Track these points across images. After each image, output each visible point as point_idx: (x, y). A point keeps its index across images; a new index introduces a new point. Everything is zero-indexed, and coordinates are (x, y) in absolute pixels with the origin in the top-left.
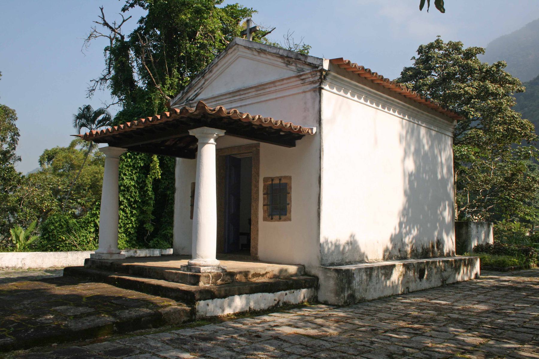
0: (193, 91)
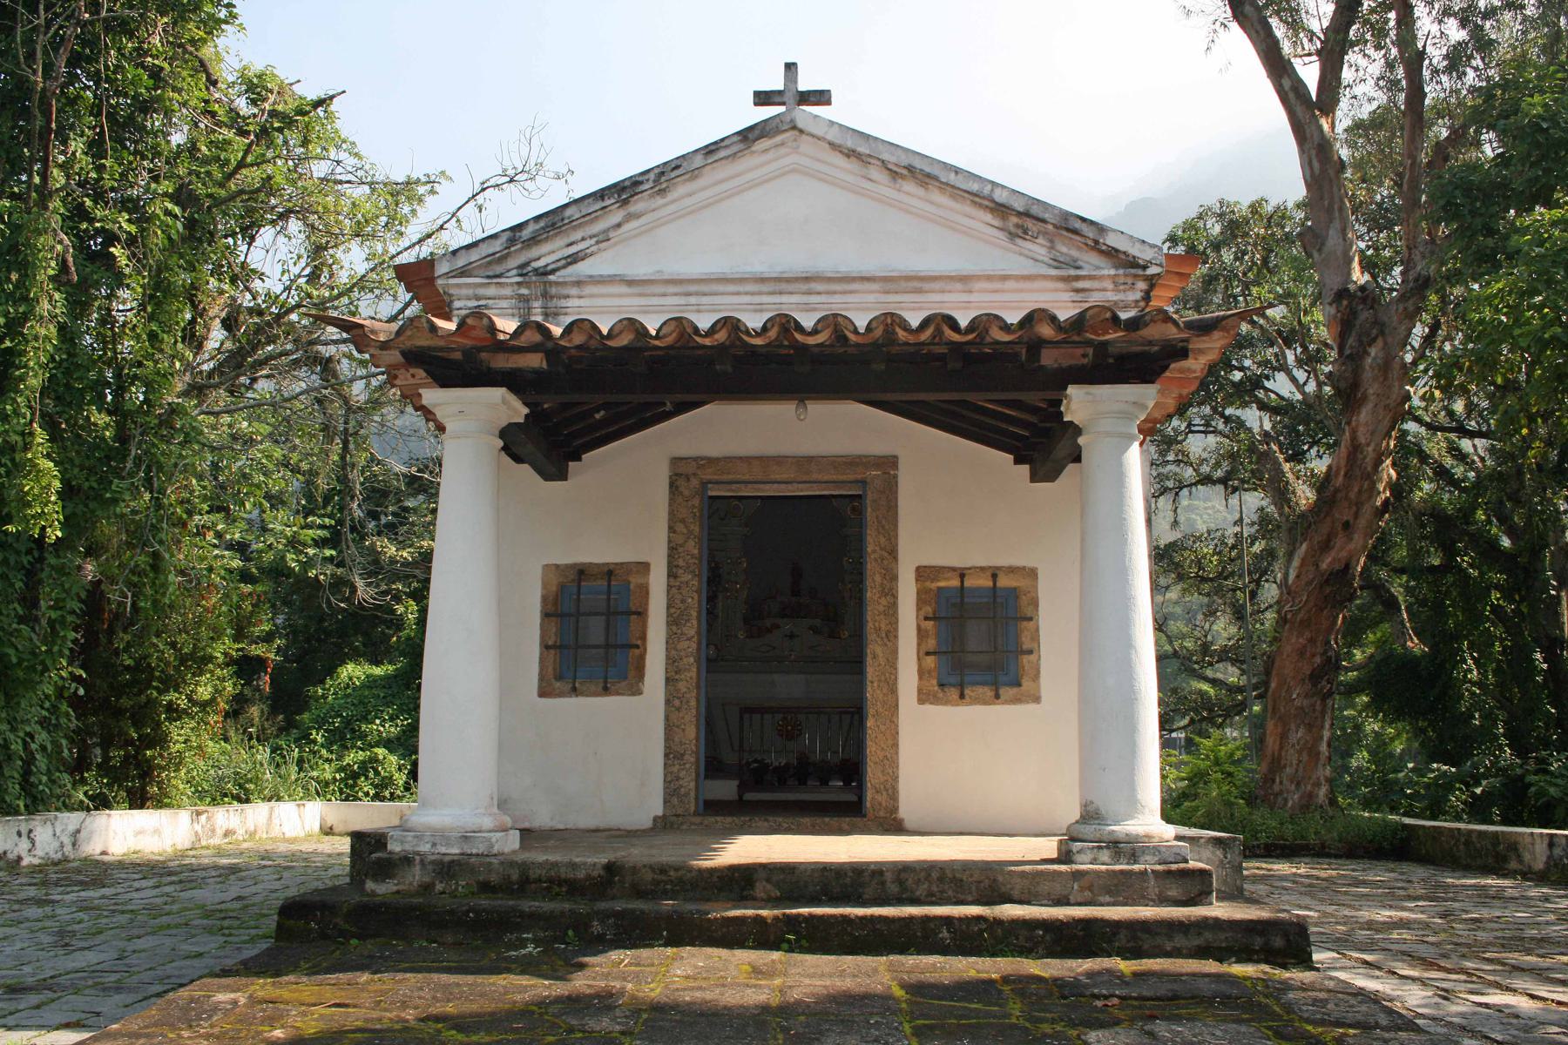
0: (559, 242)
